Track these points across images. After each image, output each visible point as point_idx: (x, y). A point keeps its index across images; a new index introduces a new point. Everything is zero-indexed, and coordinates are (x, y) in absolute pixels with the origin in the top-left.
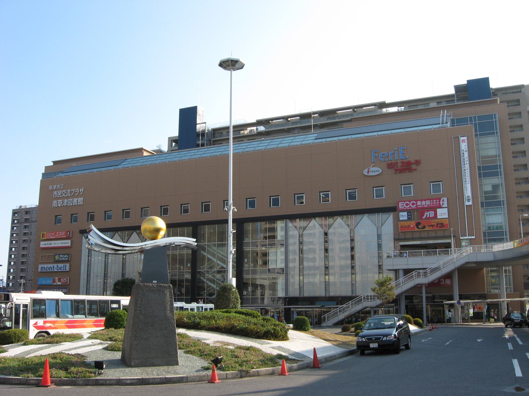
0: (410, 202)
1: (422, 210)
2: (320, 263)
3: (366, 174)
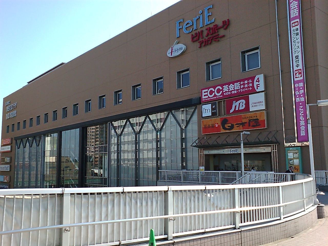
1: (230, 99)
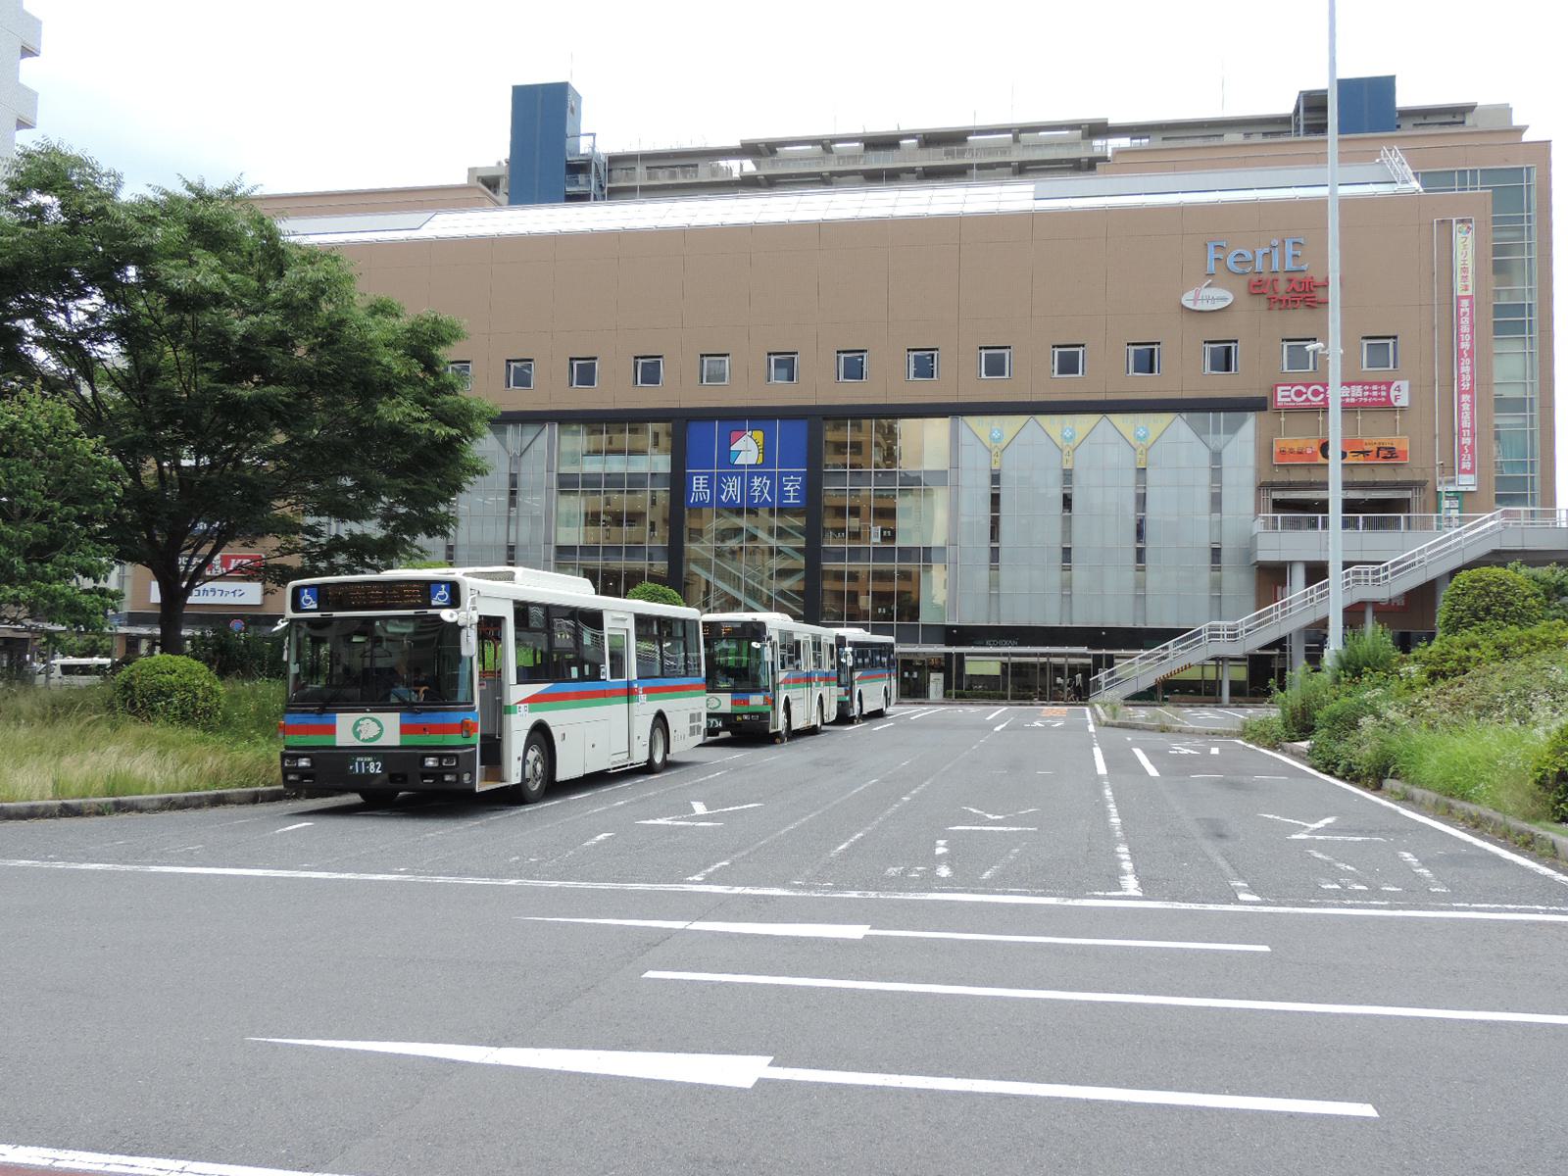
0: (1307, 386)
2: (126, 581)
3: (1189, 305)
